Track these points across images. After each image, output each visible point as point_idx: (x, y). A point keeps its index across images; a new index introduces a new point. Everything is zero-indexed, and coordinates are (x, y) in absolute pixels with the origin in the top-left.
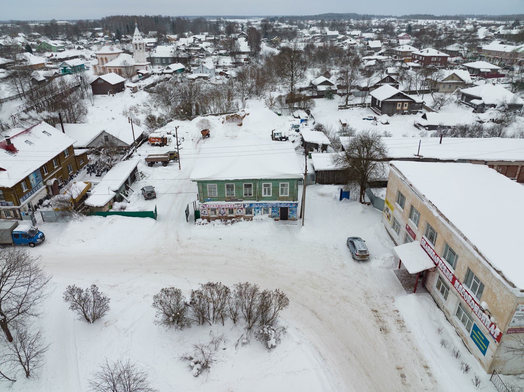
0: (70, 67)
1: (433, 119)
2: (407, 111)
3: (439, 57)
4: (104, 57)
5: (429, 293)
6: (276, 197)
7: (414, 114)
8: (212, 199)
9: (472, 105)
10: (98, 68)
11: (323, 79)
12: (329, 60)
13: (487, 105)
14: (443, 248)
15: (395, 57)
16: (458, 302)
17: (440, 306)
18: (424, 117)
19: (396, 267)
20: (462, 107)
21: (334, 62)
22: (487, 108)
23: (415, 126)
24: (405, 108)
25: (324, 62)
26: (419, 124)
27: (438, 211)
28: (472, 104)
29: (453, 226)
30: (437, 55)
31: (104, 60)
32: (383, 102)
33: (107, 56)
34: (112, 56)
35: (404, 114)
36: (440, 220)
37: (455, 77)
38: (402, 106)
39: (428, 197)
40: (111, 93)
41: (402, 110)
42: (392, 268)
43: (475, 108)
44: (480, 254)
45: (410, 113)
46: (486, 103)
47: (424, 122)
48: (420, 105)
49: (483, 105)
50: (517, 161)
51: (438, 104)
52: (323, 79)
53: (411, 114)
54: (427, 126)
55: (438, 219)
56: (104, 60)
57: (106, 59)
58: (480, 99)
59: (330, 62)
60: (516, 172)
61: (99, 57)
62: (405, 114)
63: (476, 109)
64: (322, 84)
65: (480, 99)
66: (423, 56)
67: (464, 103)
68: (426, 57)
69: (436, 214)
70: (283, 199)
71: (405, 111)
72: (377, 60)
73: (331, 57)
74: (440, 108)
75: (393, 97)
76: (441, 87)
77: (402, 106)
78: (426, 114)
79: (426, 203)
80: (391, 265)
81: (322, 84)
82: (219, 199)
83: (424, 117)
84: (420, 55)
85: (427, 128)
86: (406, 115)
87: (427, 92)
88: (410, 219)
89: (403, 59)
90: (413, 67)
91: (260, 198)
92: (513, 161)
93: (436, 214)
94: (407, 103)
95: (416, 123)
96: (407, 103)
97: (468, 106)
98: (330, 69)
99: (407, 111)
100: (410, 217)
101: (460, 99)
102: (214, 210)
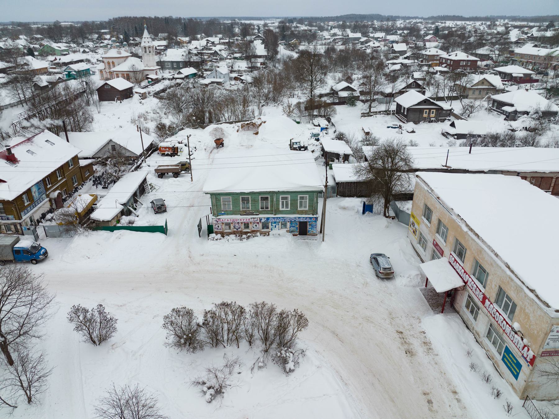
0: (75, 72)
1: (462, 127)
2: (434, 119)
3: (468, 61)
4: (111, 61)
5: (458, 313)
6: (294, 210)
7: (441, 122)
8: (227, 213)
9: (503, 113)
10: (104, 73)
11: (344, 84)
12: (351, 64)
13: (520, 112)
14: (473, 266)
15: (422, 61)
16: (488, 323)
17: (470, 327)
18: (453, 125)
19: (423, 286)
20: (493, 115)
21: (356, 66)
22: (519, 115)
23: (443, 134)
24: (432, 115)
25: (346, 66)
26: (447, 133)
27: (467, 225)
28: (504, 111)
29: (483, 241)
30: (466, 59)
31: (111, 64)
32: (409, 109)
33: (114, 60)
34: (119, 60)
35: (431, 121)
36: (469, 236)
37: (486, 83)
38: (429, 113)
39: (457, 211)
40: (118, 99)
41: (429, 117)
42: (419, 286)
43: (507, 116)
44: (512, 272)
45: (437, 121)
46: (519, 110)
47: (452, 131)
48: (448, 112)
49: (516, 112)
50: (551, 173)
51: (467, 112)
52: (344, 84)
53: (438, 121)
54: (456, 135)
55: (468, 234)
56: (111, 64)
57: (113, 63)
58: (512, 105)
59: (352, 66)
60: (551, 184)
61: (106, 61)
62: (432, 122)
63: (507, 117)
64: (344, 90)
65: (512, 105)
66: (451, 60)
67: (495, 110)
68: (454, 61)
69: (465, 229)
70: (302, 212)
71: (432, 119)
72: (402, 64)
73: (353, 61)
74: (469, 115)
75: (419, 104)
76: (470, 93)
77: (429, 113)
78: (455, 122)
79: (454, 217)
80: (417, 283)
81: (343, 90)
82: (234, 213)
83: (453, 125)
84: (448, 59)
85: (456, 137)
86: (433, 123)
87: (455, 98)
88: (437, 235)
89: (430, 63)
90: (440, 71)
91: (277, 211)
92: (547, 172)
93: (465, 229)
94: (434, 111)
95: (444, 131)
96: (434, 111)
97: (500, 114)
98: (352, 74)
99: (434, 119)
100: (438, 232)
101: (491, 105)
102: (228, 224)
